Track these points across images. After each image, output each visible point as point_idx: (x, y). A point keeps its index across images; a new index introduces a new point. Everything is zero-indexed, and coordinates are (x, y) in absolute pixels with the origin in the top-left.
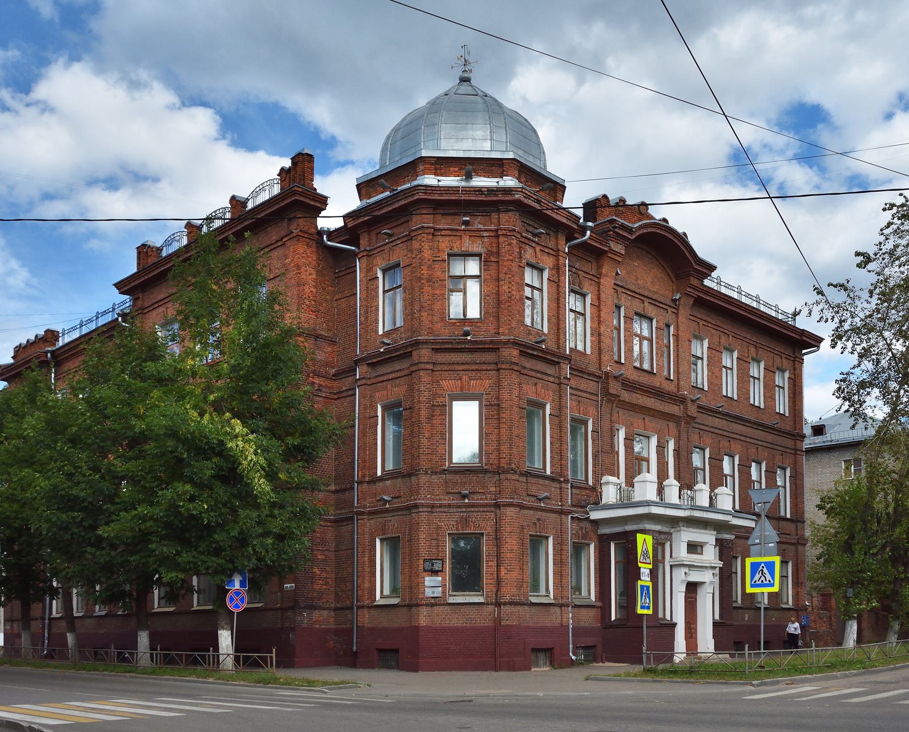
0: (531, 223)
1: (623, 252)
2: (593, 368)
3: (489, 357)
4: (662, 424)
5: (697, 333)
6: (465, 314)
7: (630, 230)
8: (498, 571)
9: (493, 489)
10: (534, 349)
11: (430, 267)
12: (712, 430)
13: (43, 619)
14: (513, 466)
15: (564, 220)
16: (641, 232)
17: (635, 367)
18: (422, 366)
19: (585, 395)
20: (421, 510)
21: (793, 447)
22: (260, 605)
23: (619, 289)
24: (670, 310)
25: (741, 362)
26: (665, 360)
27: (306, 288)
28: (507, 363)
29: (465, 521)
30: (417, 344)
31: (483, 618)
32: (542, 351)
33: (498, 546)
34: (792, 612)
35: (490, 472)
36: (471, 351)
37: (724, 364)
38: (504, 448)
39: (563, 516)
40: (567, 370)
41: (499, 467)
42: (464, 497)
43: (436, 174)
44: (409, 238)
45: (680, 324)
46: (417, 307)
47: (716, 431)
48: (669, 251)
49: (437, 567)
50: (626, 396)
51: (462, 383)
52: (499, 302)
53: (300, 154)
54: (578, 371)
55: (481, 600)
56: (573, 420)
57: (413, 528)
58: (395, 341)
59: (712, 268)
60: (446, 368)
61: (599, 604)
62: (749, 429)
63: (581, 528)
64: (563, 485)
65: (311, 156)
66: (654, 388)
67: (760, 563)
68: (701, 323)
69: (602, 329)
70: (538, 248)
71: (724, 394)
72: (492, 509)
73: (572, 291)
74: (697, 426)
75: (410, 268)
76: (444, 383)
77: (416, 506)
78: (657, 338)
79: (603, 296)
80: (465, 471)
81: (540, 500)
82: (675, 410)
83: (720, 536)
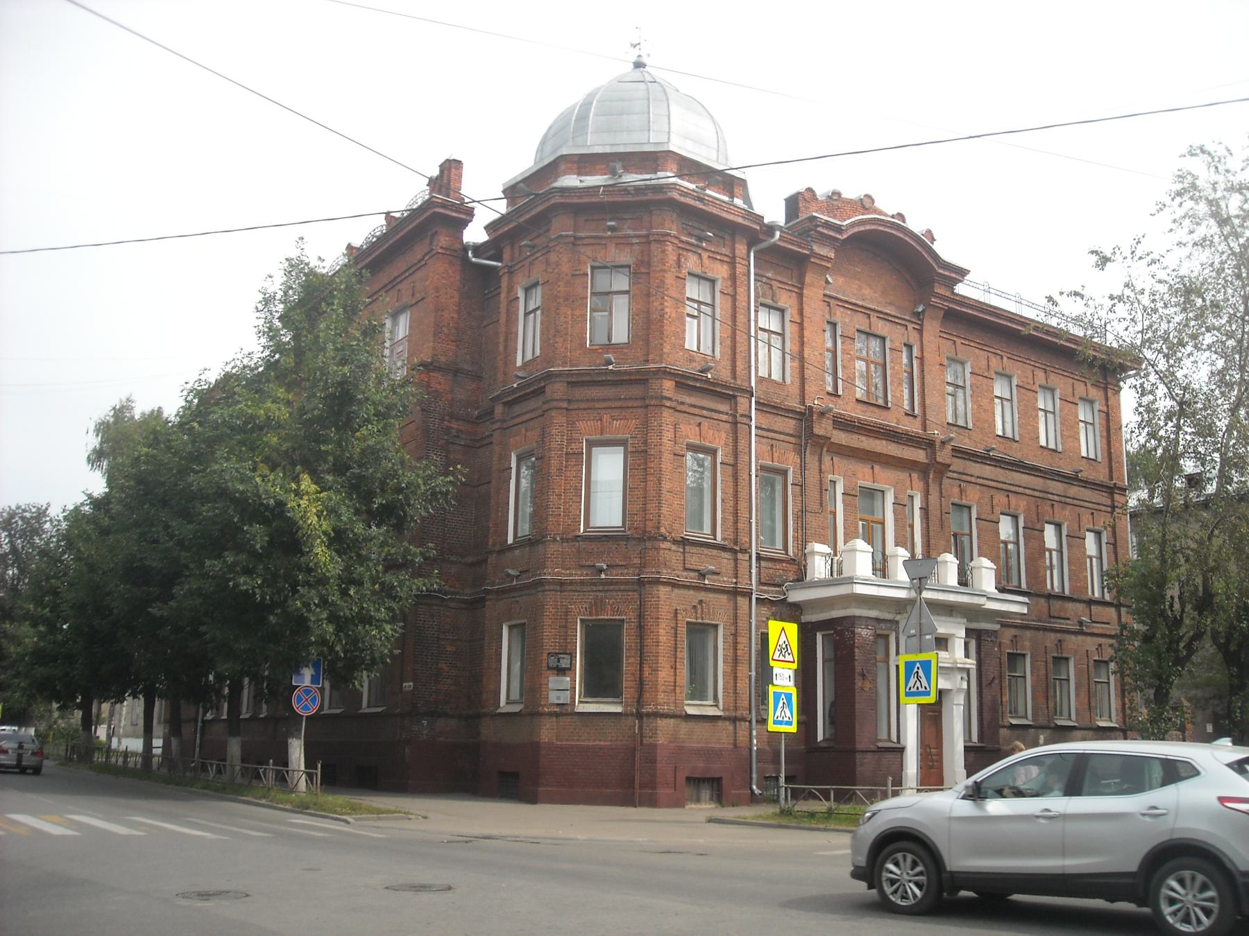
0: (696, 225)
1: (832, 255)
2: (794, 404)
3: (636, 391)
4: (903, 476)
6: (610, 339)
7: (838, 229)
9: (637, 561)
13: (197, 721)
14: (663, 530)
15: (740, 220)
16: (856, 230)
17: (828, 393)
18: (555, 404)
19: (782, 437)
20: (547, 588)
21: (1109, 503)
22: (380, 710)
23: (832, 302)
24: (910, 326)
25: (1023, 391)
26: (906, 392)
27: (446, 315)
29: (598, 605)
30: (549, 376)
32: (707, 381)
33: (641, 637)
43: (579, 174)
44: (547, 250)
46: (552, 332)
47: (986, 482)
49: (565, 663)
50: (841, 437)
53: (448, 161)
55: (618, 709)
56: (763, 468)
59: (963, 272)
60: (583, 405)
64: (740, 556)
65: (460, 162)
67: (915, 662)
70: (705, 255)
77: (541, 583)
78: (892, 362)
80: (606, 538)
82: (920, 456)
83: (974, 625)
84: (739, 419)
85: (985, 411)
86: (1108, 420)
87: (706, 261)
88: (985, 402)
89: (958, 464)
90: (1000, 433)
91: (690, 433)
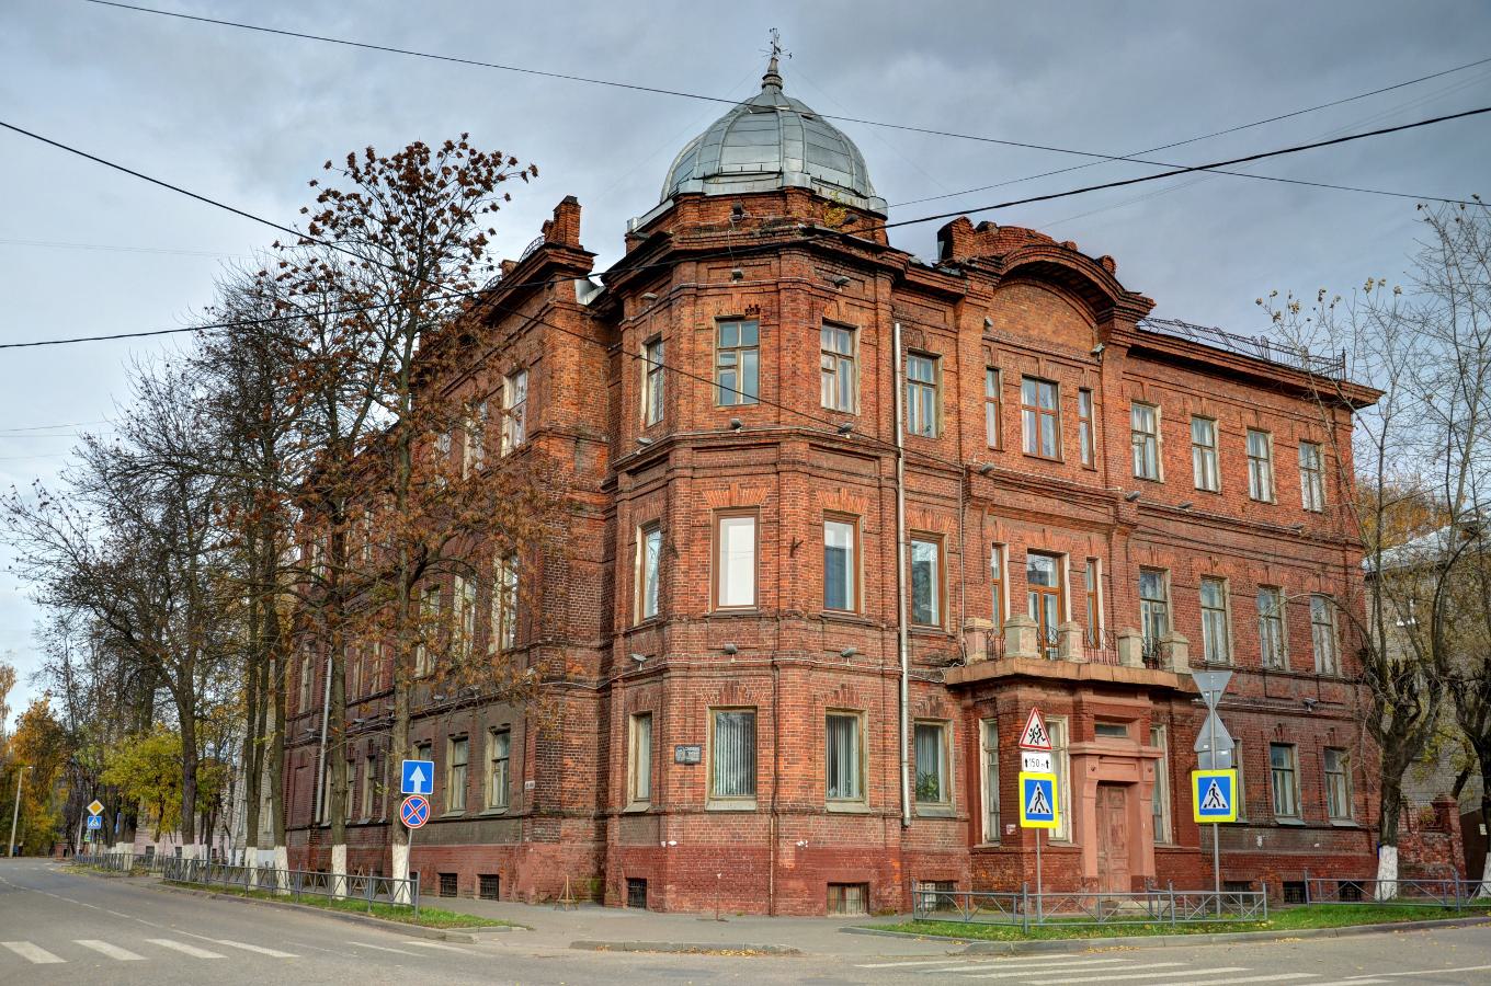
3: (769, 454)
9: (770, 643)
14: (798, 608)
19: (936, 500)
24: (1087, 368)
28: (789, 463)
29: (731, 689)
31: (755, 833)
32: (846, 442)
34: (1356, 834)
36: (743, 448)
38: (785, 583)
42: (730, 653)
44: (668, 304)
45: (1106, 388)
49: (694, 755)
50: (1005, 497)
55: (751, 805)
57: (664, 697)
59: (1149, 304)
63: (930, 698)
64: (887, 634)
67: (1210, 779)
69: (962, 405)
71: (1198, 484)
72: (770, 672)
79: (963, 358)
82: (1101, 514)
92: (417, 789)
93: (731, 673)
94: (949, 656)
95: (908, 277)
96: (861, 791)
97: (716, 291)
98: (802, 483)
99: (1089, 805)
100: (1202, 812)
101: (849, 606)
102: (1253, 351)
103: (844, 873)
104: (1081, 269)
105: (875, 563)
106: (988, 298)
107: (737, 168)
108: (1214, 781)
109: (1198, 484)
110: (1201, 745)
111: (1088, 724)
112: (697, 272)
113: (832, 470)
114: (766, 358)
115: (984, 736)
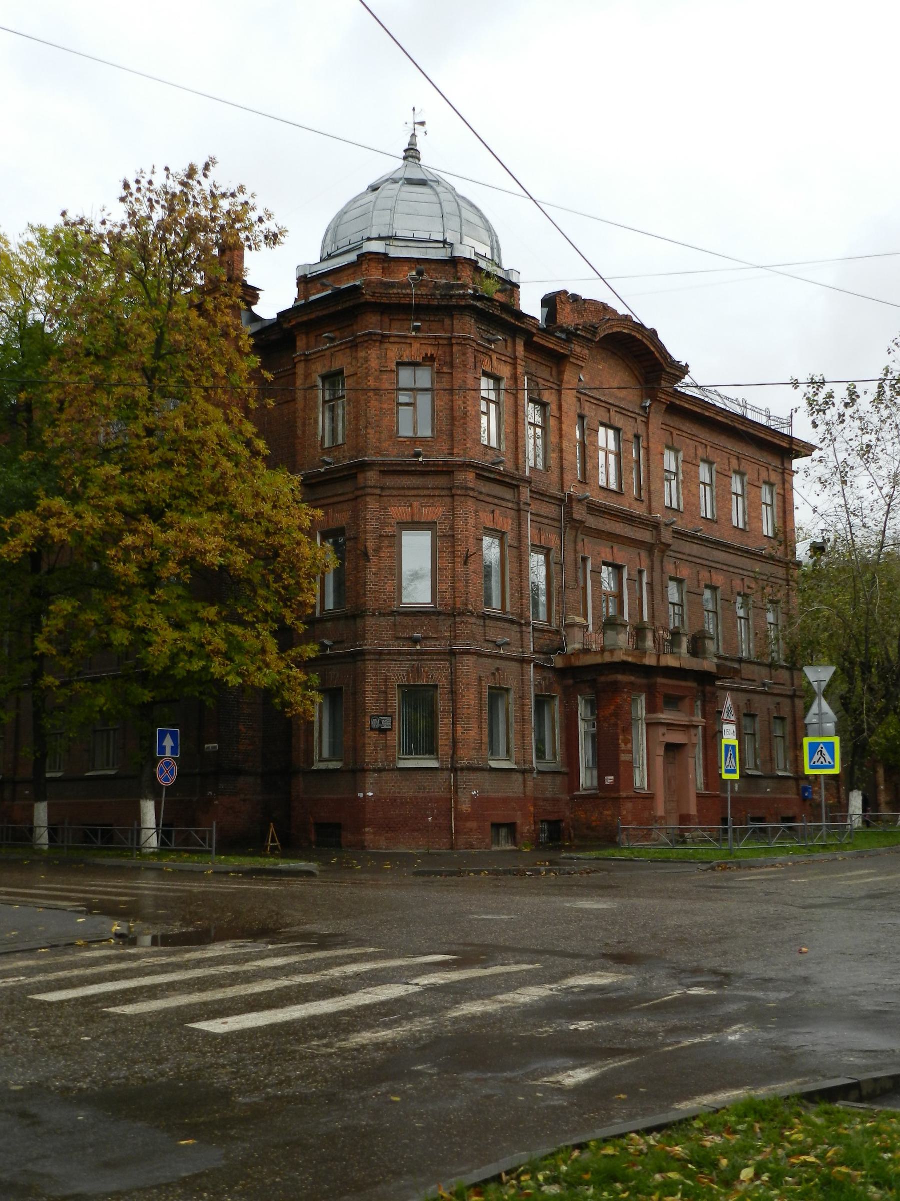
2: (555, 491)
3: (442, 481)
5: (671, 444)
8: (454, 730)
9: (448, 634)
10: (491, 472)
11: (377, 379)
12: (690, 559)
14: (470, 607)
17: (601, 487)
18: (369, 491)
20: (367, 657)
23: (583, 397)
24: (640, 419)
28: (462, 488)
31: (437, 787)
32: (499, 473)
33: (454, 701)
35: (445, 614)
37: (702, 480)
38: (460, 585)
39: (525, 665)
40: (526, 493)
41: (454, 608)
42: (416, 641)
47: (694, 560)
48: (639, 354)
49: (386, 724)
51: (412, 509)
52: (453, 419)
54: (540, 495)
55: (434, 764)
58: (338, 461)
59: (684, 370)
60: (395, 493)
61: (564, 769)
62: (732, 556)
64: (524, 628)
66: (622, 511)
67: (819, 743)
68: (675, 432)
72: (448, 657)
73: (531, 400)
74: (672, 554)
75: (355, 378)
76: (393, 511)
77: (362, 653)
79: (565, 406)
81: (499, 646)
82: (646, 536)
84: (522, 507)
85: (694, 495)
86: (784, 502)
87: (495, 363)
88: (693, 488)
89: (678, 545)
90: (486, 443)
91: (486, 519)
92: (168, 753)
93: (415, 657)
94: (556, 644)
95: (535, 339)
96: (508, 751)
97: (397, 340)
98: (471, 505)
99: (659, 762)
100: (812, 767)
101: (496, 603)
102: (739, 410)
103: (500, 816)
104: (645, 340)
105: (516, 571)
106: (584, 359)
107: (409, 234)
108: (822, 745)
109: (667, 503)
110: (811, 718)
111: (660, 700)
112: (381, 321)
113: (489, 495)
114: (441, 400)
115: (583, 709)
